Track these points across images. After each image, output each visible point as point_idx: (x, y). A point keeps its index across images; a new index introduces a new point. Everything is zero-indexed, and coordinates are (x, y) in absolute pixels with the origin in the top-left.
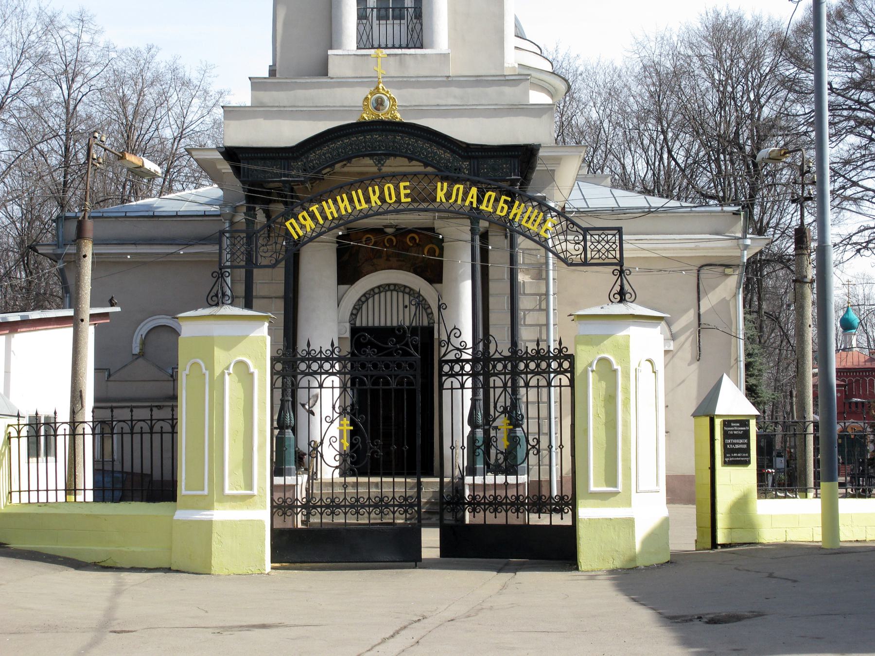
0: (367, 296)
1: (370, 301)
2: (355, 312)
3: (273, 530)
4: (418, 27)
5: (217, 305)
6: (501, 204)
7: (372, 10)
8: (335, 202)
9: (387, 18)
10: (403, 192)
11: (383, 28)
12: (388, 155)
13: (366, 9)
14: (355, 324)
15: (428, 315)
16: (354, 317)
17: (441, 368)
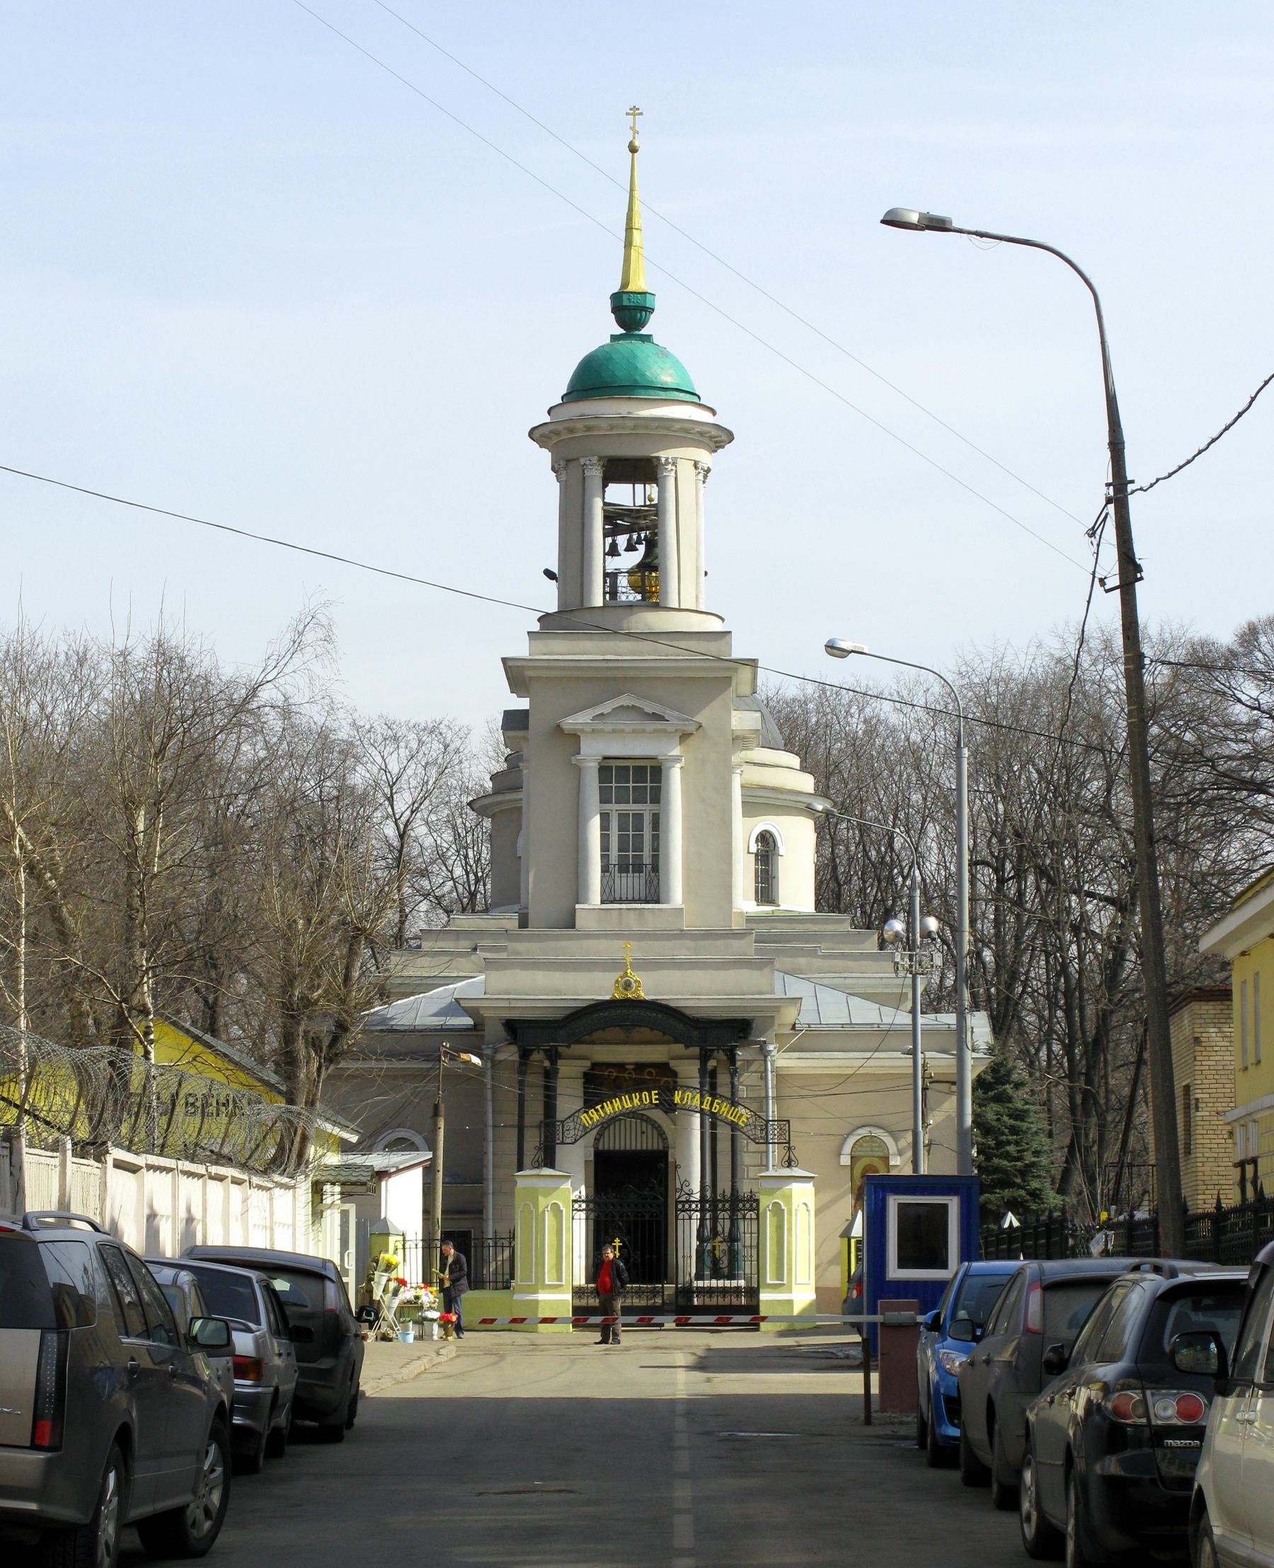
1: (612, 1127)
3: (573, 1307)
4: (655, 882)
5: (538, 1168)
6: (715, 1105)
8: (611, 1103)
9: (627, 872)
10: (654, 1097)
11: (624, 880)
12: (634, 1026)
17: (676, 1206)
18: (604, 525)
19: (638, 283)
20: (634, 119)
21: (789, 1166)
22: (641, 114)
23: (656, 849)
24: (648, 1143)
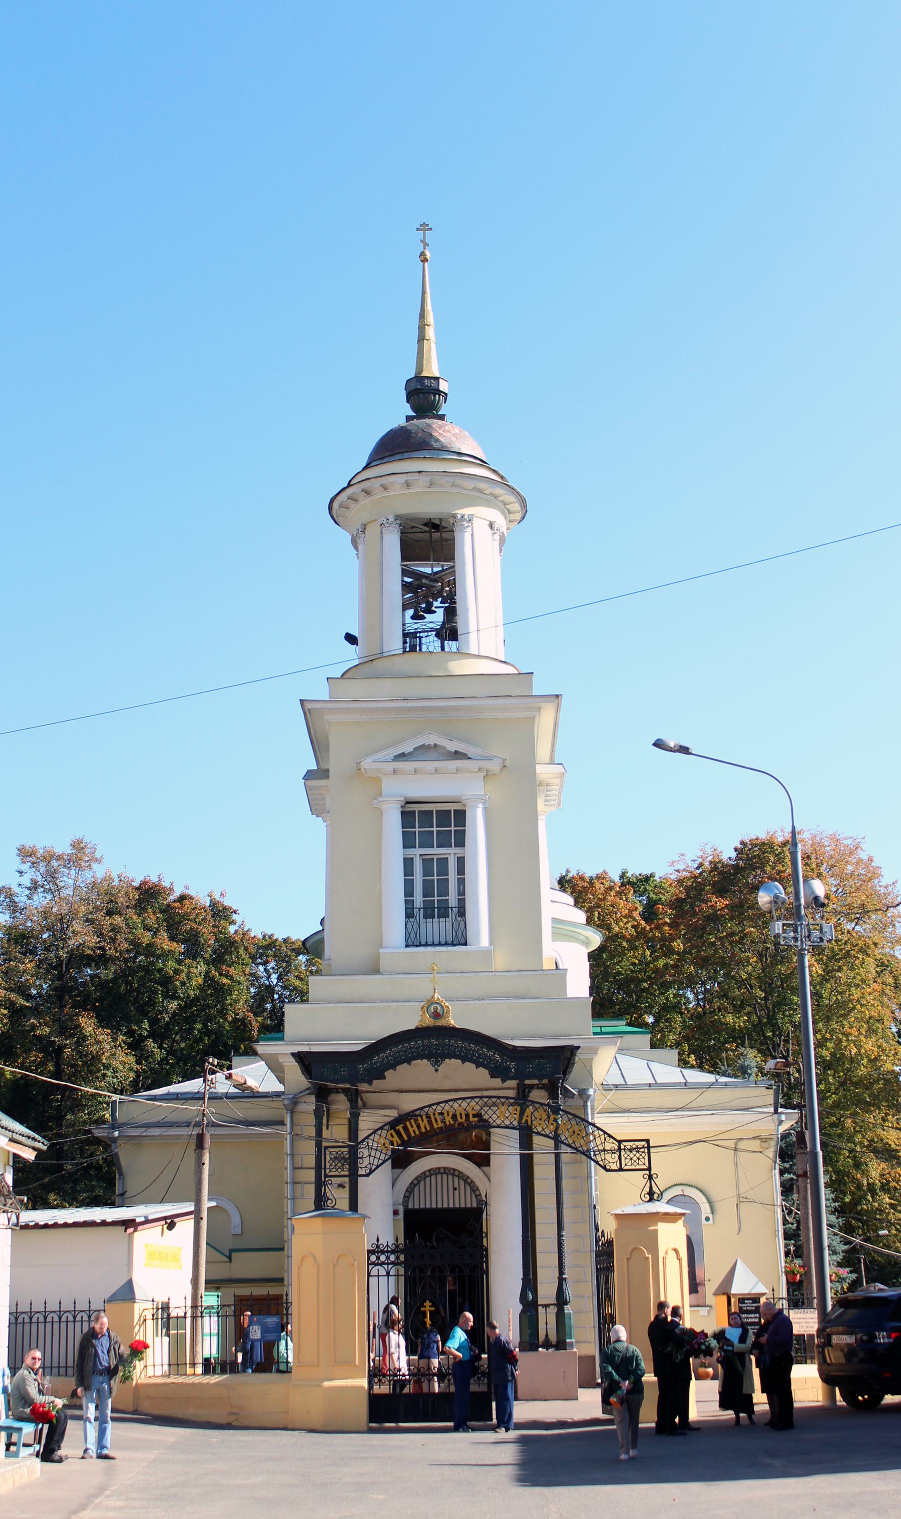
0: (419, 1179)
1: (422, 1184)
2: (407, 1194)
4: (462, 925)
7: (419, 910)
9: (433, 917)
13: (413, 908)
14: (408, 1206)
15: (476, 1196)
16: (406, 1199)
18: (403, 595)
19: (433, 369)
20: (424, 234)
21: (651, 1200)
22: (431, 229)
23: (461, 892)
24: (463, 1200)
